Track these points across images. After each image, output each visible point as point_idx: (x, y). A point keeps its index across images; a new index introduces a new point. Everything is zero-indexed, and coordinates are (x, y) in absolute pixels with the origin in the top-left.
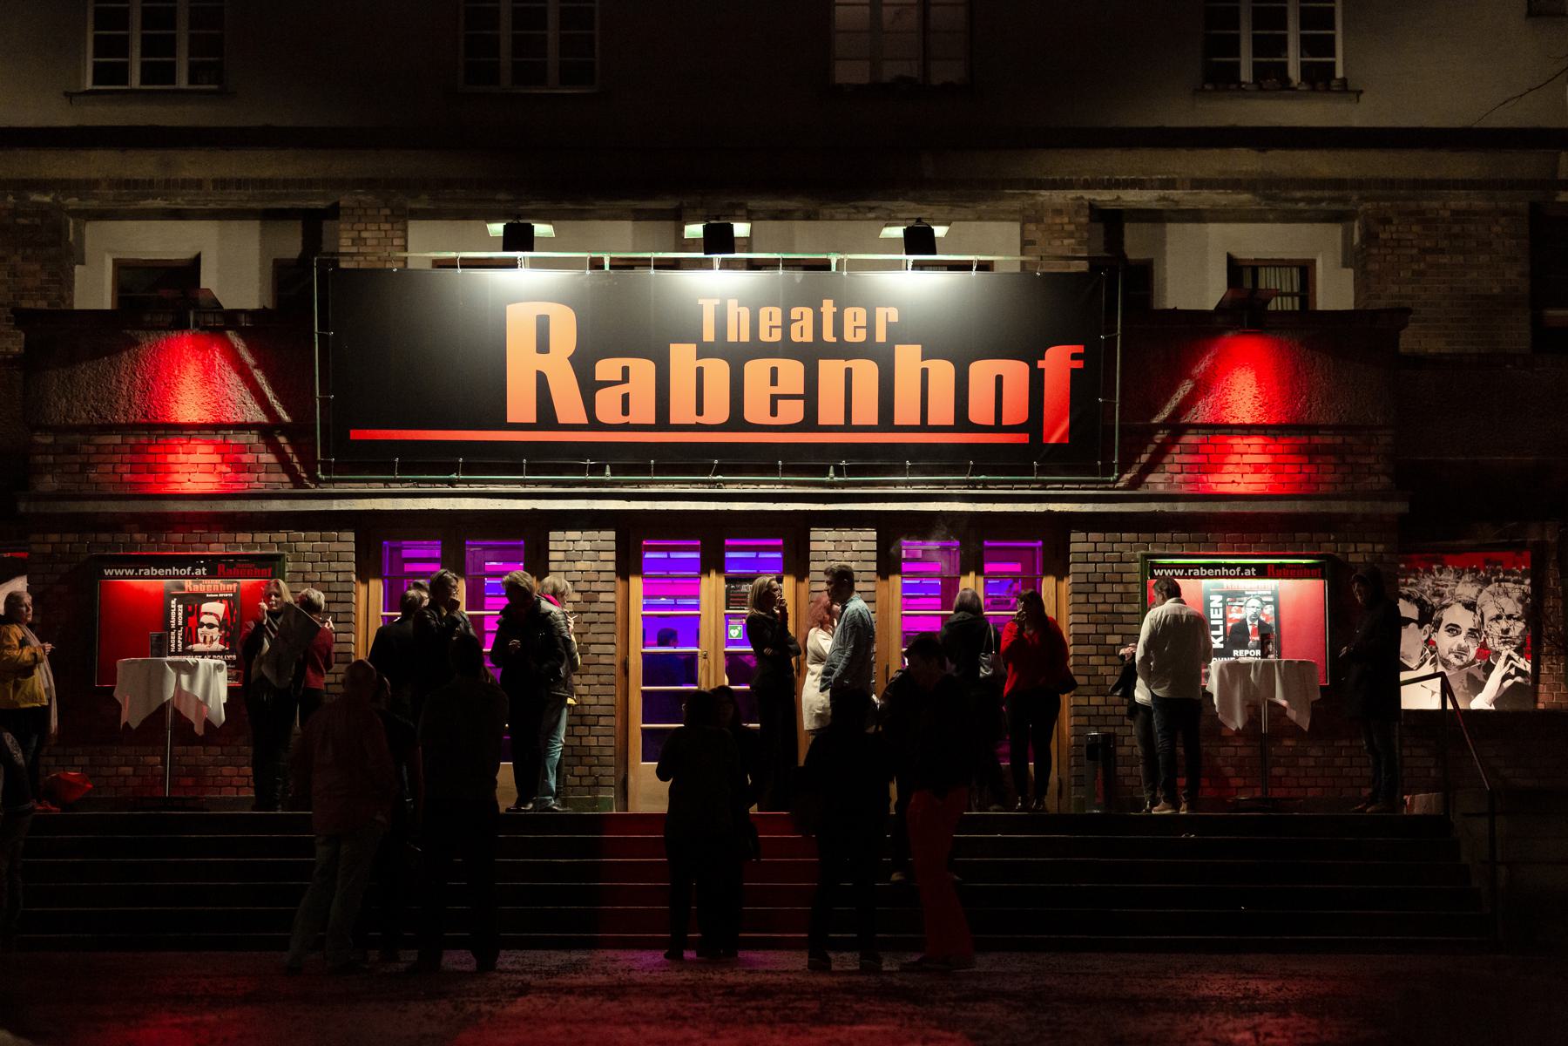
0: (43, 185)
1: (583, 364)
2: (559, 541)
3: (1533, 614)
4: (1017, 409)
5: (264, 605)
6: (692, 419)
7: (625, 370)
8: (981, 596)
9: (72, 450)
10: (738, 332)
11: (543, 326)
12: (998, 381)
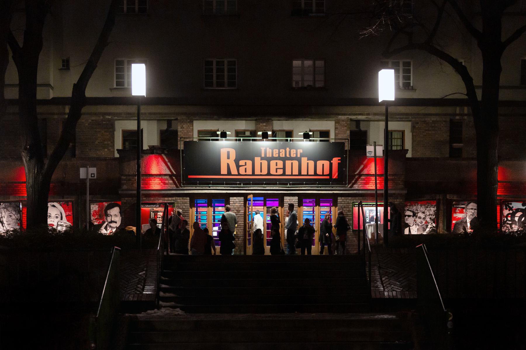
0: (109, 114)
1: (237, 161)
2: (232, 199)
3: (437, 214)
4: (327, 171)
5: (172, 213)
6: (260, 173)
7: (246, 163)
8: (262, 230)
9: (130, 180)
10: (269, 155)
11: (228, 153)
12: (323, 166)
